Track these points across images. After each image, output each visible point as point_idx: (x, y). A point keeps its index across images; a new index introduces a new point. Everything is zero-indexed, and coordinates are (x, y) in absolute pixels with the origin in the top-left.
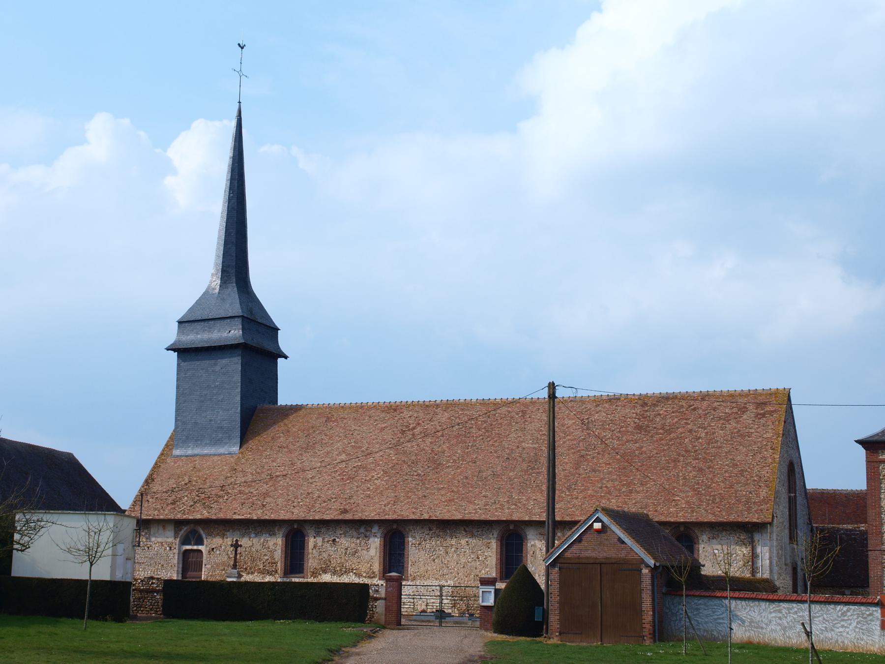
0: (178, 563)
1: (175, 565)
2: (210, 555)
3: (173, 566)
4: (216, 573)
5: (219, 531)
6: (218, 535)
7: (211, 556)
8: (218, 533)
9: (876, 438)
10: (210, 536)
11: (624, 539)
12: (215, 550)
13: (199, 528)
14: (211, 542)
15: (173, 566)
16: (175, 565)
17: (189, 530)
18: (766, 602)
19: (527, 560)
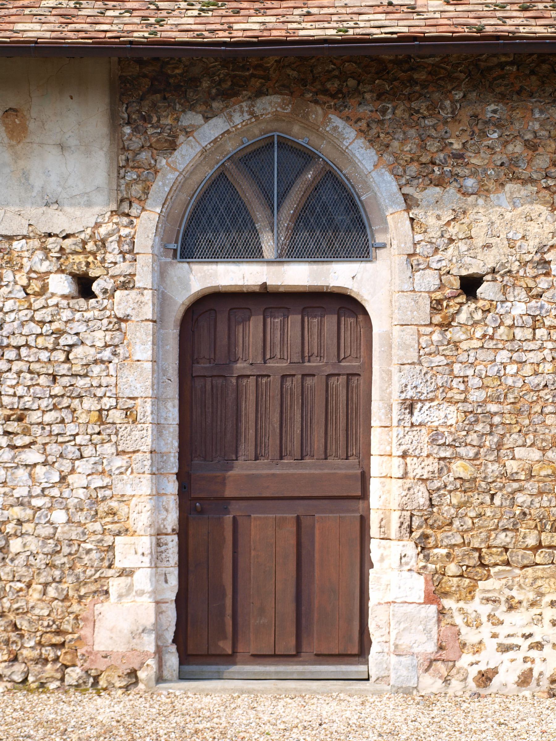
0: (158, 399)
1: (129, 412)
2: (446, 325)
3: (116, 416)
4: (512, 466)
5: (517, 148)
6: (515, 178)
7: (455, 333)
8: (514, 161)
9: (366, 631)
10: (439, 183)
11: (172, 509)
12: (485, 291)
13: (337, 121)
14: (453, 230)
15: (116, 416)
16: (129, 412)
17: (231, 147)
18: (303, 313)
19: (152, 430)
